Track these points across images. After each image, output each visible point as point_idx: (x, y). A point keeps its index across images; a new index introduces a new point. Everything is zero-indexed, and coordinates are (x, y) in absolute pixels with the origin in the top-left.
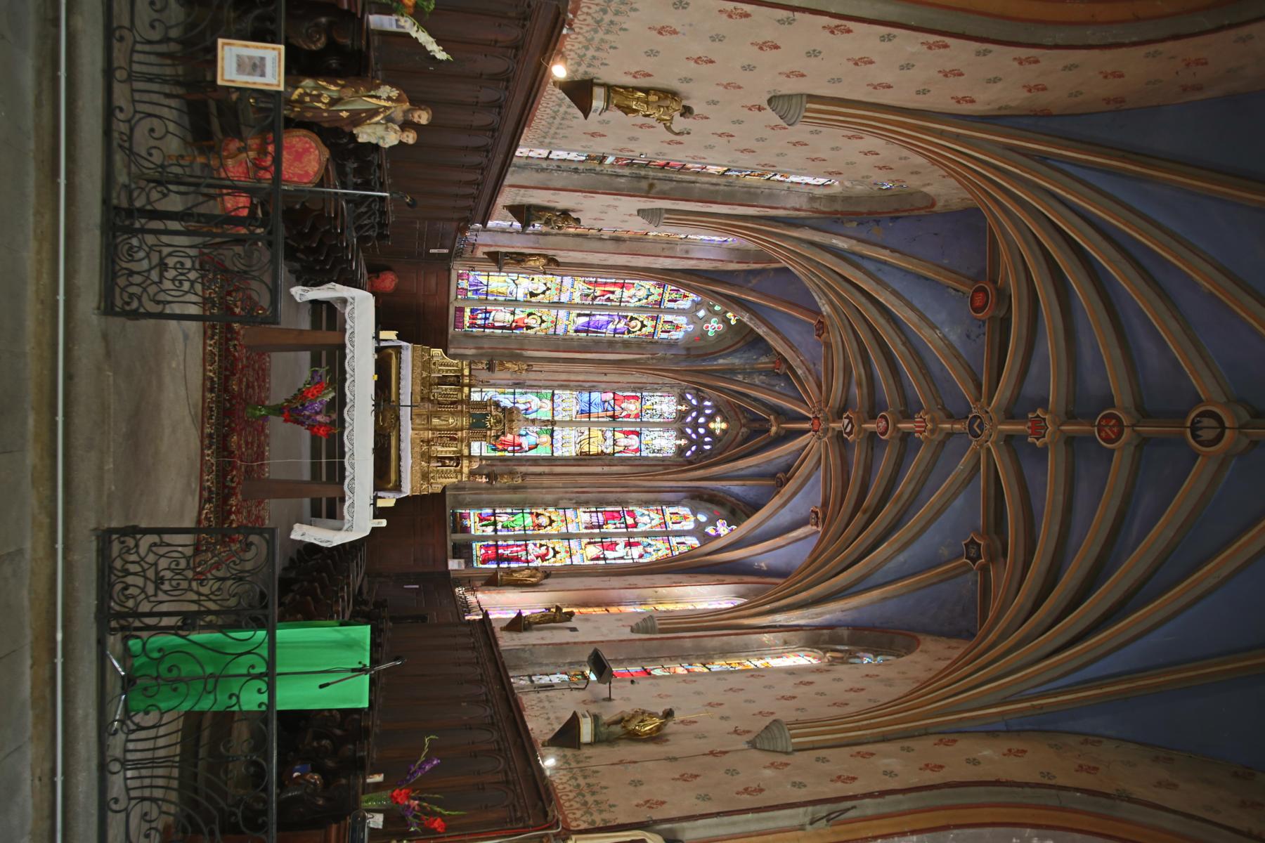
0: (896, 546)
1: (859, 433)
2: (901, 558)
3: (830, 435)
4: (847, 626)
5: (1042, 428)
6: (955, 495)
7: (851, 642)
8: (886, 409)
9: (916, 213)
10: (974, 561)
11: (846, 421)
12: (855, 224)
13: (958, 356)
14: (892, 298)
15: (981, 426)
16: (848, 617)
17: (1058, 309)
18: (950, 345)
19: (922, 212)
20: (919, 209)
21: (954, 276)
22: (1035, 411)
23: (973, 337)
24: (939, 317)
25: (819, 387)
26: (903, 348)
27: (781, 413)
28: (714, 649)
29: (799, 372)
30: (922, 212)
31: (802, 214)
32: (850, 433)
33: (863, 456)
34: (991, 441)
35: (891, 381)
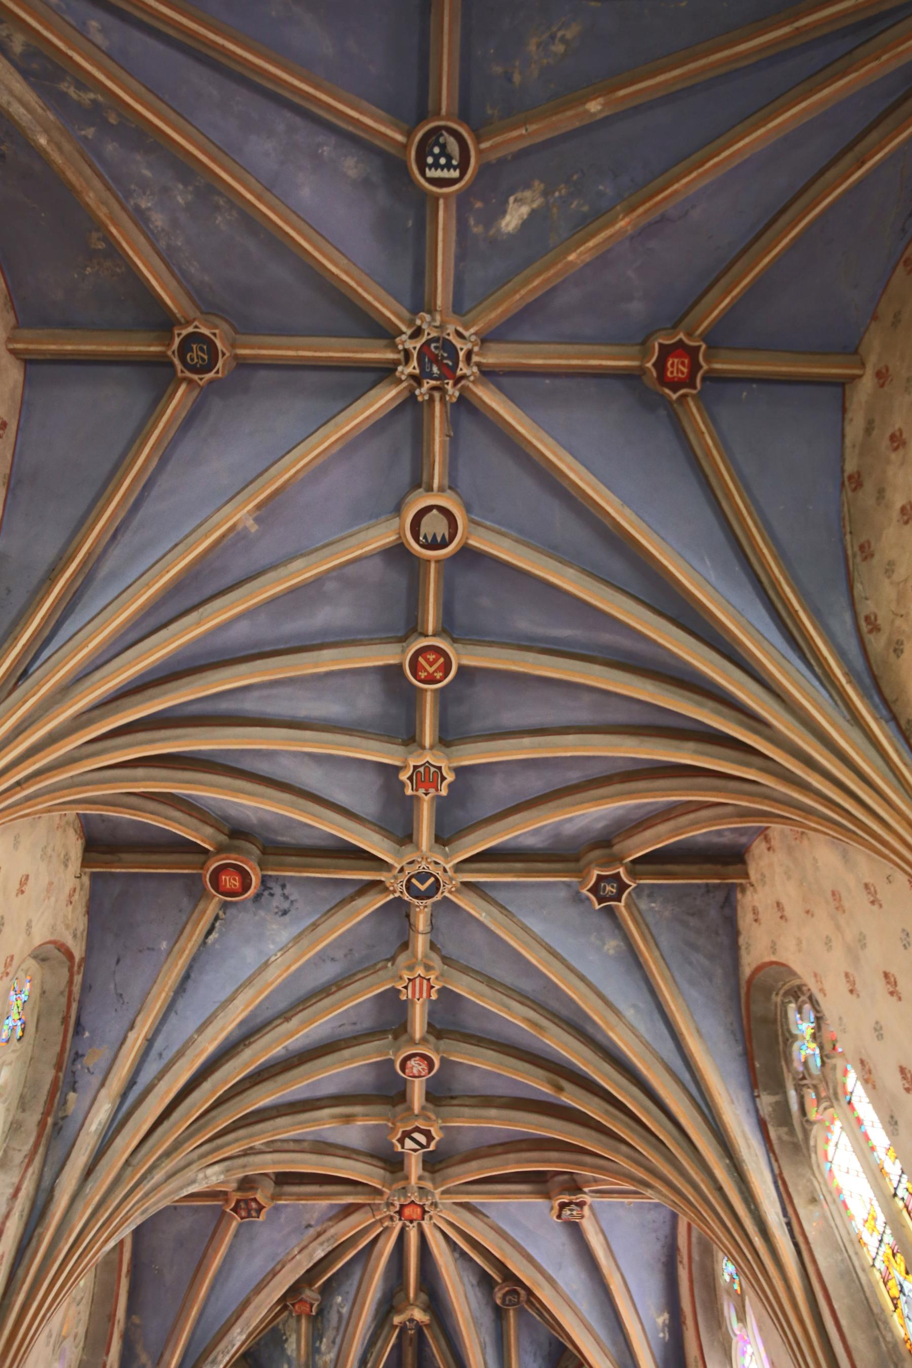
0: (613, 1018)
1: (428, 1119)
2: (629, 1013)
3: (428, 1185)
4: (754, 1098)
5: (427, 769)
6: (525, 929)
7: (778, 1087)
8: (391, 1062)
9: (76, 989)
10: (623, 887)
11: (409, 1143)
12: (72, 1096)
13: (315, 926)
14: (210, 1031)
15: (423, 877)
16: (742, 1097)
17: (258, 729)
18: (297, 939)
19: (78, 979)
20: (71, 982)
21: (189, 928)
22: (403, 784)
23: (286, 905)
24: (250, 956)
25: (348, 1210)
26: (295, 1021)
27: (389, 1304)
28: (876, 1342)
29: (320, 1254)
30: (78, 979)
31: (28, 1187)
32: (428, 1134)
33: (466, 1111)
34: (442, 863)
35: (346, 1053)
